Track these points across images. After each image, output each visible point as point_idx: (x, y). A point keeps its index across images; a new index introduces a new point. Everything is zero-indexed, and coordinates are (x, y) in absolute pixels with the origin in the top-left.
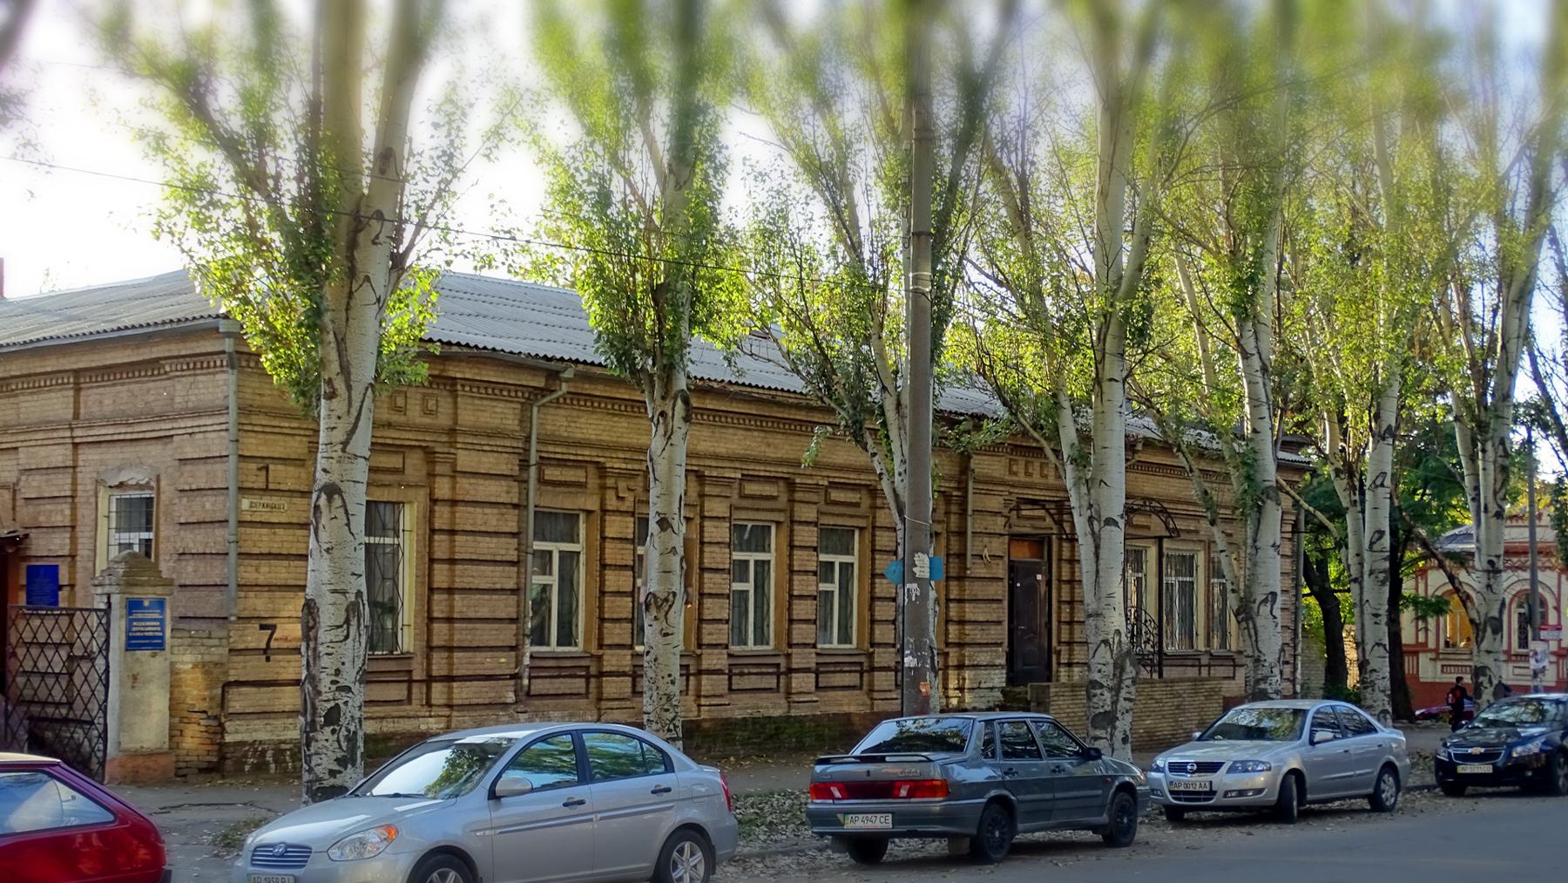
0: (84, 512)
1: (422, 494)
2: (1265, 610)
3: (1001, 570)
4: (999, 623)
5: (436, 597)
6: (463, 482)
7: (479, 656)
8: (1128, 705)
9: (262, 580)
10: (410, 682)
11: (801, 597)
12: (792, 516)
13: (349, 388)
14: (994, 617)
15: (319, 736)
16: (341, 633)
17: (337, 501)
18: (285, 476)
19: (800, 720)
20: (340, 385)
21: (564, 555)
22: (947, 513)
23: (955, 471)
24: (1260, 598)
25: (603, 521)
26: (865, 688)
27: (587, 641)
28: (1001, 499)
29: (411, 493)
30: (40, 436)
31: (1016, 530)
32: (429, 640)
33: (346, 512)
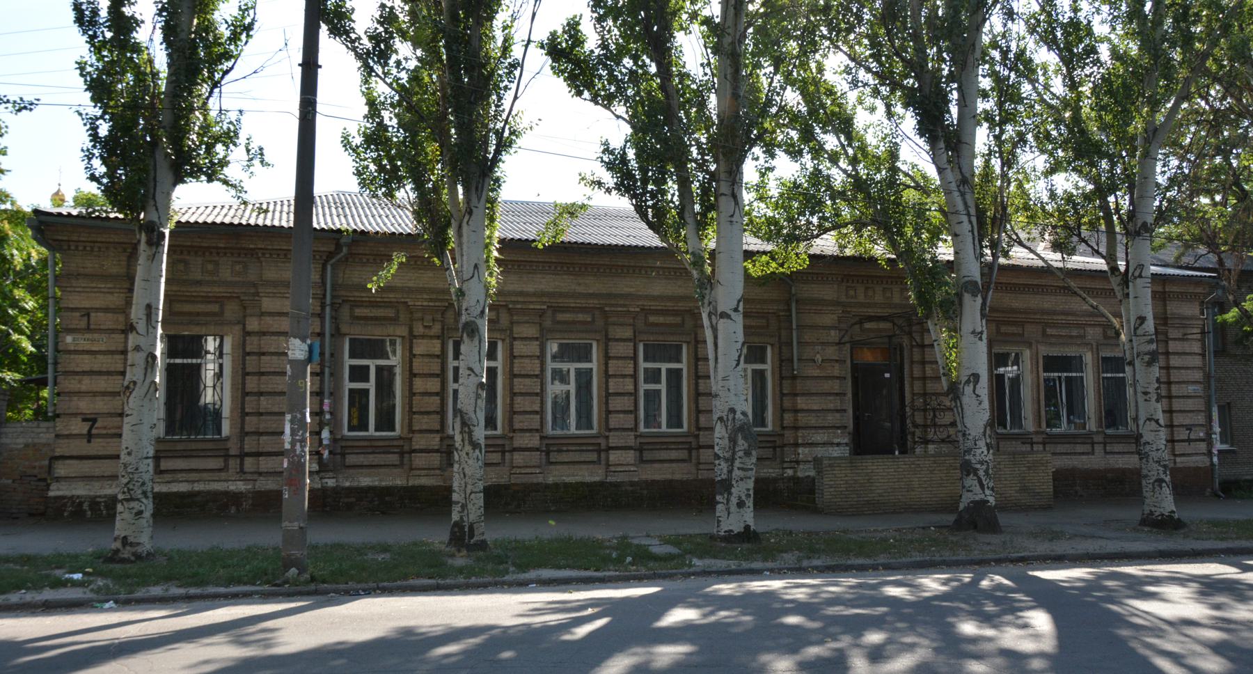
2: (968, 389)
9: (84, 388)
12: (606, 335)
18: (107, 320)
19: (616, 485)
24: (964, 379)
26: (603, 462)
27: (774, 425)
28: (835, 317)
32: (242, 428)
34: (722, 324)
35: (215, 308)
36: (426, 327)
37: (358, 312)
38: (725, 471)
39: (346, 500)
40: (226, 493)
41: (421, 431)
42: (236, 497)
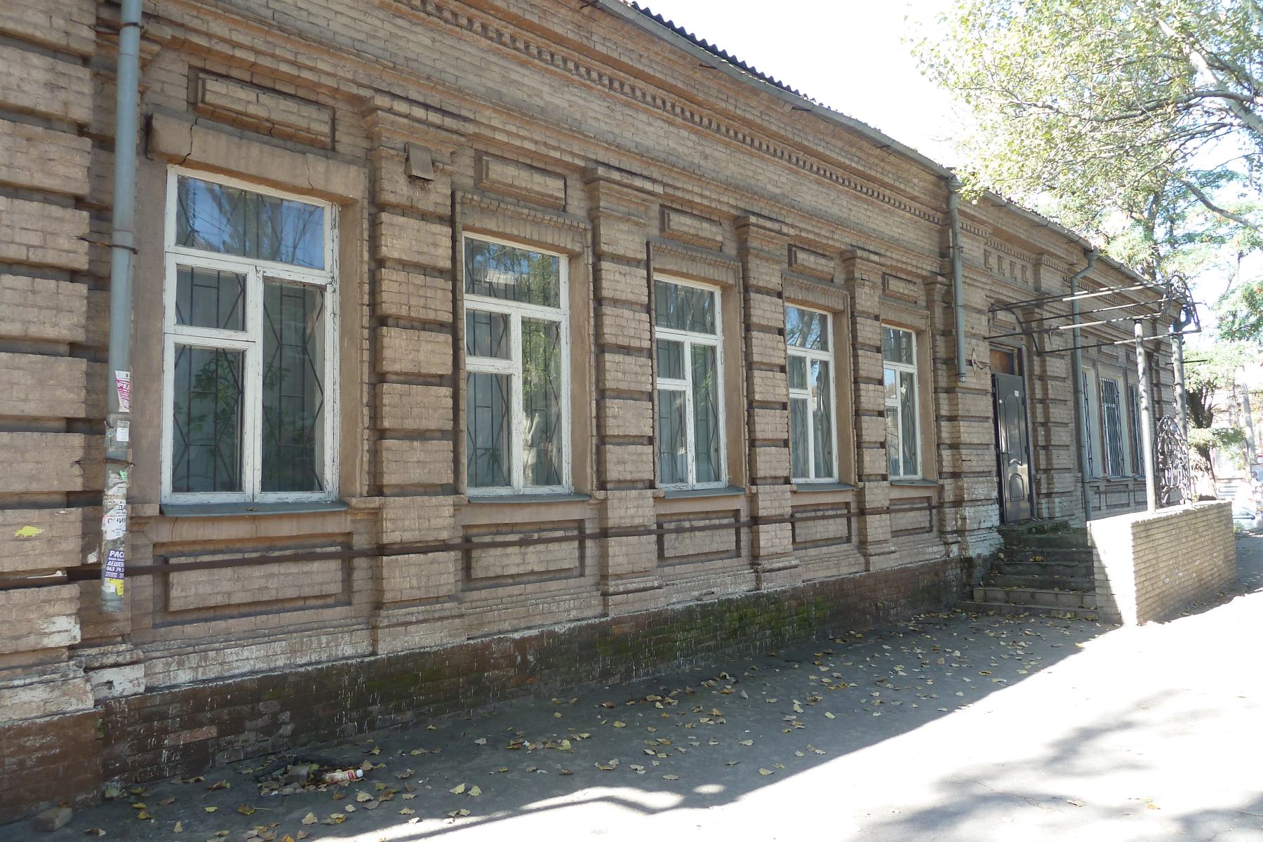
21: (277, 293)
25: (375, 225)
26: (854, 539)
36: (413, 179)
37: (218, 93)
39: (185, 737)
41: (403, 491)
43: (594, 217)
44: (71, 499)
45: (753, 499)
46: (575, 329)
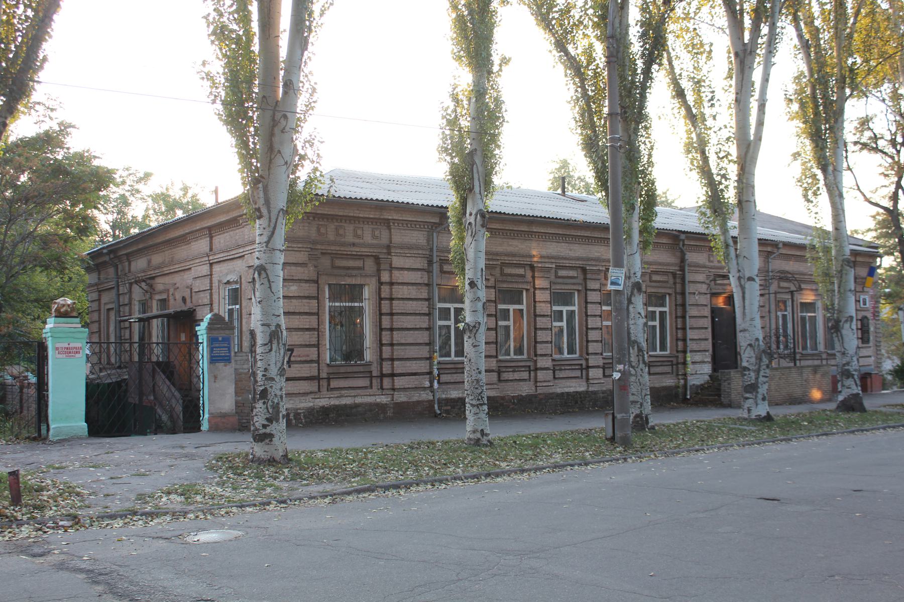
0: (215, 297)
1: (374, 281)
2: (847, 326)
3: (707, 312)
4: (706, 339)
5: (383, 333)
6: (396, 273)
7: (408, 363)
8: (765, 379)
10: (371, 377)
11: (592, 329)
13: (269, 212)
14: (703, 337)
15: (257, 406)
16: (268, 348)
17: (264, 275)
19: (594, 393)
20: (264, 211)
22: (675, 283)
23: (678, 261)
27: (671, 350)
28: (704, 275)
29: (368, 280)
30: (197, 261)
31: (714, 291)
33: (269, 281)
34: (748, 285)
35: (358, 263)
38: (753, 378)
40: (377, 405)
42: (382, 407)
43: (533, 277)
44: (427, 359)
45: (587, 360)
46: (528, 311)
